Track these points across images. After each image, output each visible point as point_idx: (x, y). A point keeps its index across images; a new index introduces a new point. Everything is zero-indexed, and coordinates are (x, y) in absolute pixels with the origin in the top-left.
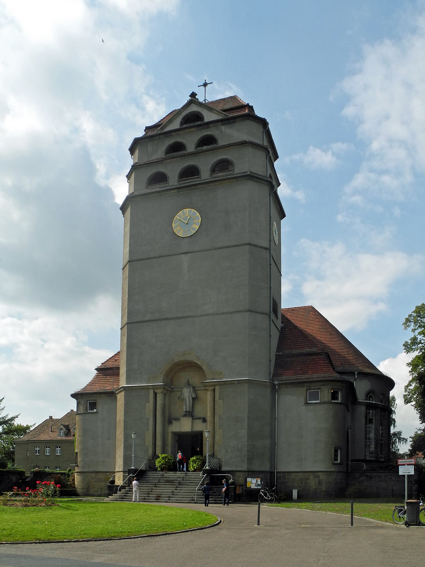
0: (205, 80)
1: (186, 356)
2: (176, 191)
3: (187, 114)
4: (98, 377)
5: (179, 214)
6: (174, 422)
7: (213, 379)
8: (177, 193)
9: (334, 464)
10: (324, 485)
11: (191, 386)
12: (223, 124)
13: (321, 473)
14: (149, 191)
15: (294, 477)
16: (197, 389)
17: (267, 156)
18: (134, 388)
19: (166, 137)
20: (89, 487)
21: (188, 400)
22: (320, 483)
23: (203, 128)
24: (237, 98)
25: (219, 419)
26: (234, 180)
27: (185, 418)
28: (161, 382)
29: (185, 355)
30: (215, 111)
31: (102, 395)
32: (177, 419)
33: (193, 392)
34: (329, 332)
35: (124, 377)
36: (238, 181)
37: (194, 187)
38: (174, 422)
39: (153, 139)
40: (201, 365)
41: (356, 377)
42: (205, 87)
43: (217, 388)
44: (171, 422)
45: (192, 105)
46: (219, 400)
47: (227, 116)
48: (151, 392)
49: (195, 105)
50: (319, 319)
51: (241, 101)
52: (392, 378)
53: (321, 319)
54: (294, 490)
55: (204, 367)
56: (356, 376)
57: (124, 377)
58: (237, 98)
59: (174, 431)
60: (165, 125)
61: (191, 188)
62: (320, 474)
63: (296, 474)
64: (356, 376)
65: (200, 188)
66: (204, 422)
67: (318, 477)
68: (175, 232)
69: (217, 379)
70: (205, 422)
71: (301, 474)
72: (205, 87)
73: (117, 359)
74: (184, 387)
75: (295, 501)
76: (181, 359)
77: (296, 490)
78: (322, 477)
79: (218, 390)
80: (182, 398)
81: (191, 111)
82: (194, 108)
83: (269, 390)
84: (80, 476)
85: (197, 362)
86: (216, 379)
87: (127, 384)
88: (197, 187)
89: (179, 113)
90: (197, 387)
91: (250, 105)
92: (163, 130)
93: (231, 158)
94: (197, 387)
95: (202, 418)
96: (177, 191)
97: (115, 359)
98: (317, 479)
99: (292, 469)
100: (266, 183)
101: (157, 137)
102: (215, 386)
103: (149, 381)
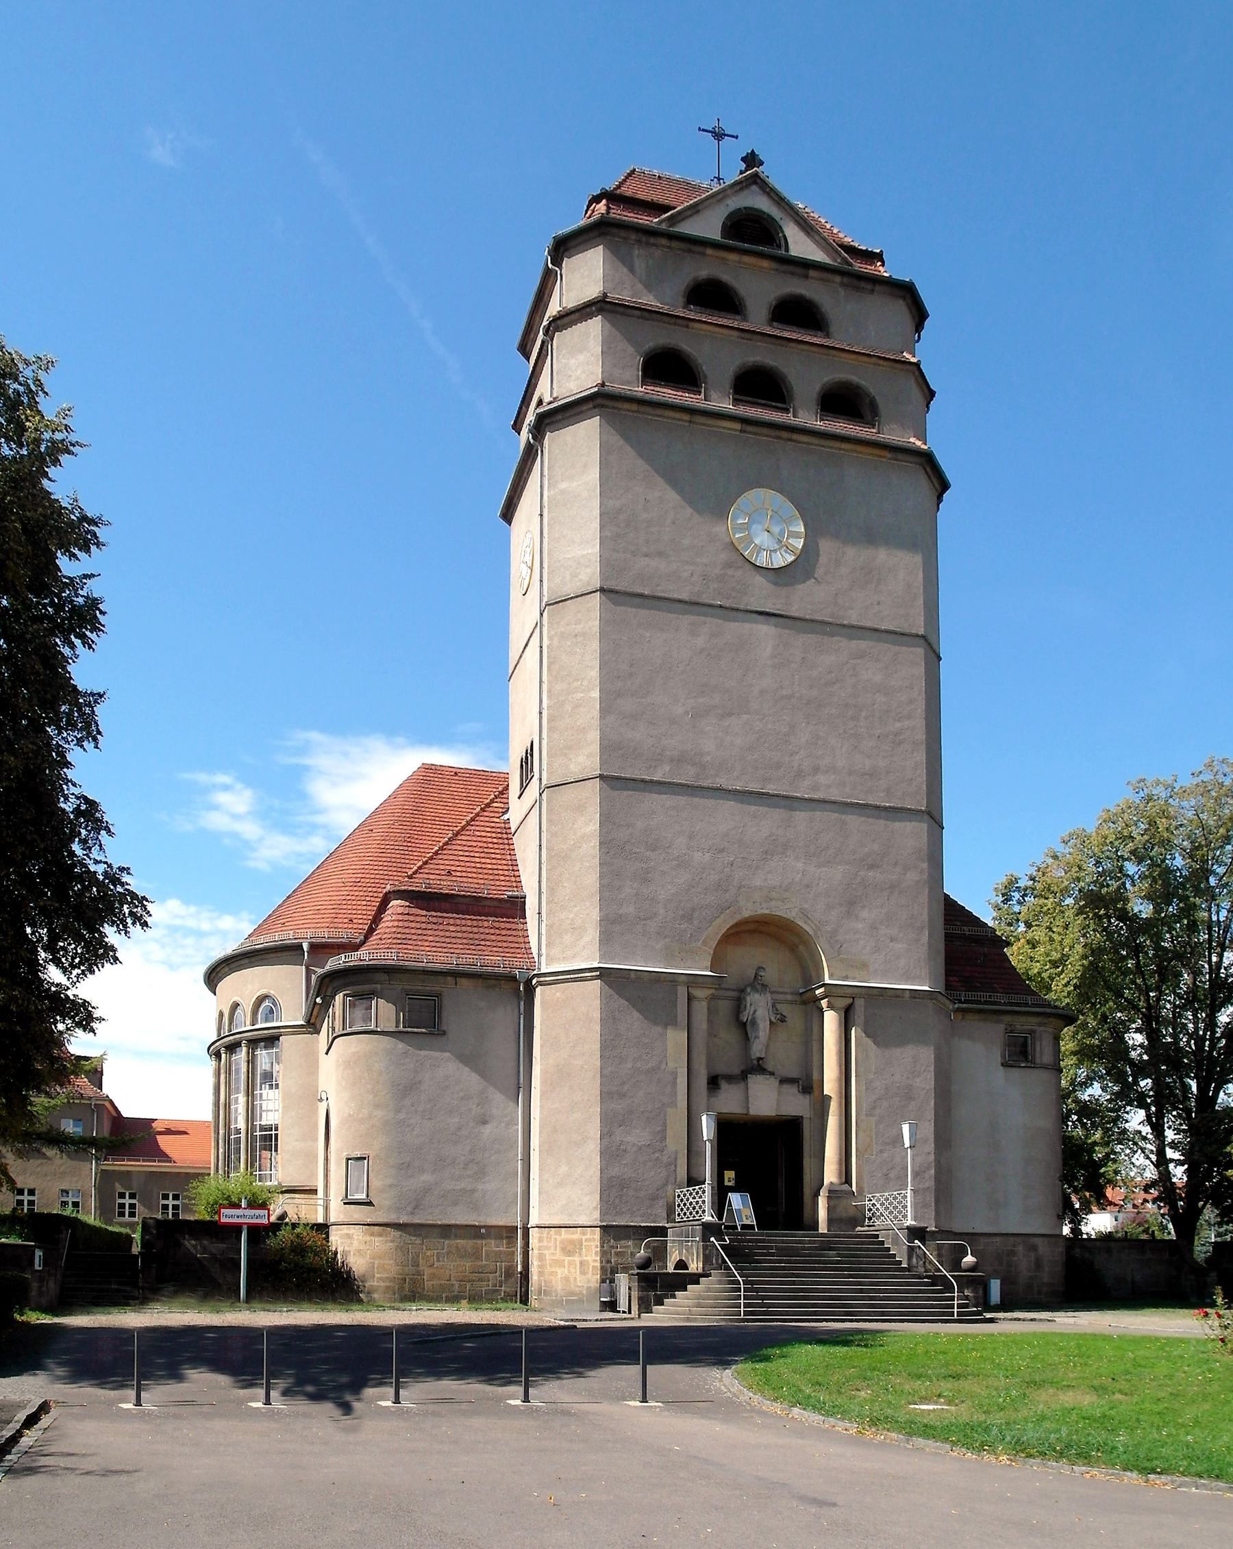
1: (773, 903)
2: (738, 426)
7: (846, 978)
8: (737, 433)
10: (1047, 1269)
12: (842, 285)
13: (1041, 1239)
14: (652, 396)
15: (982, 1248)
18: (700, 979)
19: (690, 251)
20: (419, 1273)
22: (1038, 1264)
23: (792, 274)
25: (867, 1089)
26: (889, 455)
28: (705, 969)
29: (771, 900)
30: (817, 238)
31: (464, 982)
36: (897, 460)
37: (785, 434)
39: (652, 240)
42: (719, 140)
43: (860, 1003)
45: (754, 187)
47: (851, 265)
48: (682, 992)
60: (679, 213)
61: (777, 433)
62: (1038, 1241)
63: (987, 1240)
65: (800, 442)
67: (1034, 1248)
69: (854, 979)
71: (998, 1239)
74: (749, 990)
76: (760, 912)
77: (998, 1281)
79: (863, 1008)
84: (381, 1239)
86: (854, 978)
88: (795, 436)
92: (672, 225)
96: (739, 428)
98: (1033, 1255)
101: (664, 241)
102: (853, 998)
103: (669, 959)
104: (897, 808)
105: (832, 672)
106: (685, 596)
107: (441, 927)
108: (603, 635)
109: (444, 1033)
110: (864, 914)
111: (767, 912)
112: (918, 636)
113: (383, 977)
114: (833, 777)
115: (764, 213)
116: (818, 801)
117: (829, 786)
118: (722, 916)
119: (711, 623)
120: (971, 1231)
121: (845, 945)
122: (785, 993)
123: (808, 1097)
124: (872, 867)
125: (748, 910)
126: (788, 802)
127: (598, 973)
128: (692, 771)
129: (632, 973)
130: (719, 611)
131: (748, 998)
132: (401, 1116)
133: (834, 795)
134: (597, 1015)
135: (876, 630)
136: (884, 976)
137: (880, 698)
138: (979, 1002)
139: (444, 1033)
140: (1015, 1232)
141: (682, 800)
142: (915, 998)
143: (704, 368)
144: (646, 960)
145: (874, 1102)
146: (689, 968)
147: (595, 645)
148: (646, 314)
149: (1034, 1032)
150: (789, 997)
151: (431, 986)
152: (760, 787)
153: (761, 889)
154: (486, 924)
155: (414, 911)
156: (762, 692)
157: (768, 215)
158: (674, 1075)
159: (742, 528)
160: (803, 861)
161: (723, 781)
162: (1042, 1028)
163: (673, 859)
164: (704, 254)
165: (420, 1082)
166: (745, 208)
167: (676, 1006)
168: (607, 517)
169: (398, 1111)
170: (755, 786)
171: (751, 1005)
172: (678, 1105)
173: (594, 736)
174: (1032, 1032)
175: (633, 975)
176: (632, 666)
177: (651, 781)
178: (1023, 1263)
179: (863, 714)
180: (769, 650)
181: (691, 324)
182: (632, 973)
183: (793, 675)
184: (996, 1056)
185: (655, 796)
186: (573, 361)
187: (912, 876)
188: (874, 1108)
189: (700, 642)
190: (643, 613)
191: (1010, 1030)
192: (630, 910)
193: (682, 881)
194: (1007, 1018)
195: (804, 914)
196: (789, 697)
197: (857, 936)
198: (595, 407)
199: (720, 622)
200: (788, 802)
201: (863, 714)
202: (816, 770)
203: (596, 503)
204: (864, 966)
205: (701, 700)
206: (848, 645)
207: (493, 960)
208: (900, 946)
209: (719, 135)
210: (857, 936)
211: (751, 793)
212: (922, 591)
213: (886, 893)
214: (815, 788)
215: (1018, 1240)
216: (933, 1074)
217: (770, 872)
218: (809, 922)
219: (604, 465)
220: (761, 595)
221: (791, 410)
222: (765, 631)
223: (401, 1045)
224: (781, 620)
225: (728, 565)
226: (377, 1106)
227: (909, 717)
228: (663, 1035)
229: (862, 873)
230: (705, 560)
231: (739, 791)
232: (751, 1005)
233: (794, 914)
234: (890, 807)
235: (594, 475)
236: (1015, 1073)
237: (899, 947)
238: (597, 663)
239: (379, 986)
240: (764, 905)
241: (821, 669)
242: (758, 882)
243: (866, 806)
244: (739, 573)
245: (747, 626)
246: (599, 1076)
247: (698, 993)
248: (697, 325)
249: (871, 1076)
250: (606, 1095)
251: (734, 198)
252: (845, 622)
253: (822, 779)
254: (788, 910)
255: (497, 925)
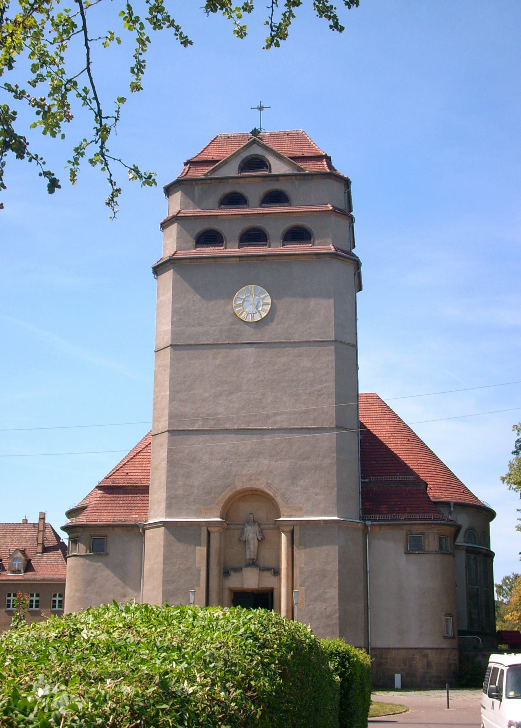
0: (261, 102)
1: (252, 482)
2: (238, 259)
3: (248, 157)
4: (103, 499)
5: (241, 290)
6: (232, 573)
7: (291, 516)
9: (445, 637)
11: (257, 524)
12: (296, 179)
15: (394, 656)
16: (263, 526)
17: (350, 224)
19: (221, 182)
21: (252, 542)
22: (429, 664)
24: (314, 145)
25: (300, 573)
27: (249, 569)
28: (217, 517)
32: (238, 570)
33: (259, 531)
34: (406, 438)
35: (162, 507)
38: (232, 573)
40: (273, 497)
41: (452, 510)
42: (261, 111)
44: (228, 573)
45: (255, 145)
46: (300, 545)
49: (258, 146)
50: (389, 416)
51: (312, 143)
52: (493, 508)
53: (391, 416)
54: (396, 675)
55: (278, 500)
56: (452, 508)
57: (162, 507)
58: (305, 135)
59: (232, 586)
62: (429, 651)
64: (452, 508)
66: (275, 575)
67: (426, 656)
68: (237, 314)
69: (295, 516)
70: (277, 575)
71: (404, 651)
72: (261, 111)
73: (128, 471)
74: (246, 524)
75: (397, 690)
77: (400, 675)
78: (432, 656)
80: (244, 540)
81: (253, 154)
82: (256, 151)
83: (360, 534)
85: (267, 491)
87: (167, 516)
89: (237, 154)
90: (263, 524)
91: (328, 155)
93: (310, 226)
94: (263, 524)
95: (273, 570)
97: (125, 471)
98: (425, 659)
99: (392, 644)
100: (352, 262)
104: (319, 428)
105: (285, 366)
106: (210, 342)
107: (116, 502)
108: (172, 365)
109: (107, 554)
110: (301, 483)
111: (249, 486)
112: (330, 341)
113: (81, 529)
114: (285, 416)
115: (259, 155)
116: (276, 429)
117: (283, 421)
118: (226, 490)
119: (223, 352)
120: (388, 647)
121: (290, 500)
122: (269, 524)
123: (276, 577)
124: (304, 459)
125: (239, 486)
126: (261, 431)
127: (162, 524)
128: (212, 422)
129: (179, 523)
130: (228, 346)
131: (246, 529)
132: (87, 595)
133: (286, 425)
134: (162, 543)
135: (308, 342)
136: (312, 514)
137: (311, 374)
138: (388, 520)
139: (107, 554)
140: (414, 647)
141: (207, 437)
142: (326, 524)
143: (225, 235)
144: (188, 515)
145: (304, 579)
146: (209, 517)
147: (168, 371)
148: (197, 217)
149: (425, 533)
150: (271, 526)
151: (102, 532)
152: (247, 426)
153: (246, 475)
154: (138, 498)
155: (106, 495)
156: (248, 381)
157: (262, 156)
158: (199, 570)
159: (239, 306)
160: (268, 459)
161: (228, 426)
162: (429, 531)
163: (202, 466)
164: (228, 182)
165: (96, 578)
166: (250, 156)
167: (201, 537)
168: (175, 312)
169: (85, 593)
170: (244, 426)
171: (247, 532)
172: (201, 586)
173: (167, 412)
174: (422, 534)
175: (179, 523)
176: (184, 377)
177: (193, 430)
178: (419, 664)
179: (301, 384)
180: (252, 360)
181: (218, 217)
182: (179, 523)
183: (265, 370)
184: (401, 547)
185: (194, 437)
186: (168, 242)
187: (327, 461)
188: (304, 582)
189: (218, 362)
190: (192, 352)
191: (409, 534)
192: (180, 492)
193: (206, 476)
194: (406, 528)
195: (268, 485)
196: (263, 381)
197: (297, 494)
198: (171, 264)
199: (228, 350)
200: (261, 431)
201: (301, 384)
202: (276, 414)
203: (171, 305)
204: (301, 509)
205: (219, 389)
206: (292, 351)
207: (134, 517)
208: (321, 497)
209: (261, 108)
210: (297, 494)
211: (241, 429)
212: (333, 319)
213: (313, 471)
214: (275, 423)
215: (416, 651)
216: (338, 563)
217: (251, 467)
218: (272, 490)
219: (174, 288)
220: (250, 335)
221: (268, 244)
222: (250, 350)
223: (87, 561)
224: (259, 345)
225: (232, 324)
226: (77, 591)
227: (326, 381)
228: (195, 550)
229: (300, 462)
230: (222, 323)
231: (236, 430)
232: (247, 532)
233: (263, 486)
234: (315, 428)
235: (170, 294)
236: (413, 557)
237: (319, 497)
238: (168, 379)
239: (79, 534)
240: (247, 483)
241: (279, 365)
242: (244, 472)
243: (302, 429)
244: (237, 327)
245: (242, 350)
246: (162, 573)
247: (211, 529)
248: (221, 217)
249: (303, 566)
250: (165, 582)
251: (245, 153)
252: (292, 341)
253: (279, 418)
254: (261, 485)
255: (143, 498)
